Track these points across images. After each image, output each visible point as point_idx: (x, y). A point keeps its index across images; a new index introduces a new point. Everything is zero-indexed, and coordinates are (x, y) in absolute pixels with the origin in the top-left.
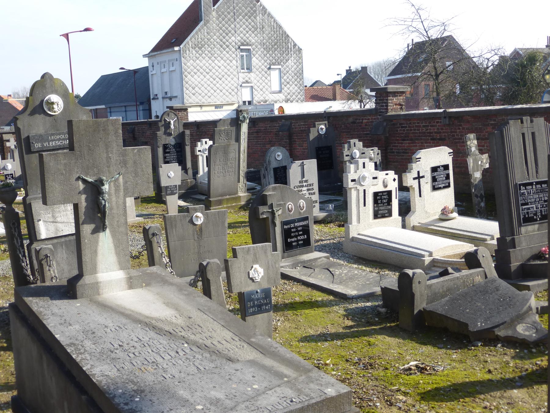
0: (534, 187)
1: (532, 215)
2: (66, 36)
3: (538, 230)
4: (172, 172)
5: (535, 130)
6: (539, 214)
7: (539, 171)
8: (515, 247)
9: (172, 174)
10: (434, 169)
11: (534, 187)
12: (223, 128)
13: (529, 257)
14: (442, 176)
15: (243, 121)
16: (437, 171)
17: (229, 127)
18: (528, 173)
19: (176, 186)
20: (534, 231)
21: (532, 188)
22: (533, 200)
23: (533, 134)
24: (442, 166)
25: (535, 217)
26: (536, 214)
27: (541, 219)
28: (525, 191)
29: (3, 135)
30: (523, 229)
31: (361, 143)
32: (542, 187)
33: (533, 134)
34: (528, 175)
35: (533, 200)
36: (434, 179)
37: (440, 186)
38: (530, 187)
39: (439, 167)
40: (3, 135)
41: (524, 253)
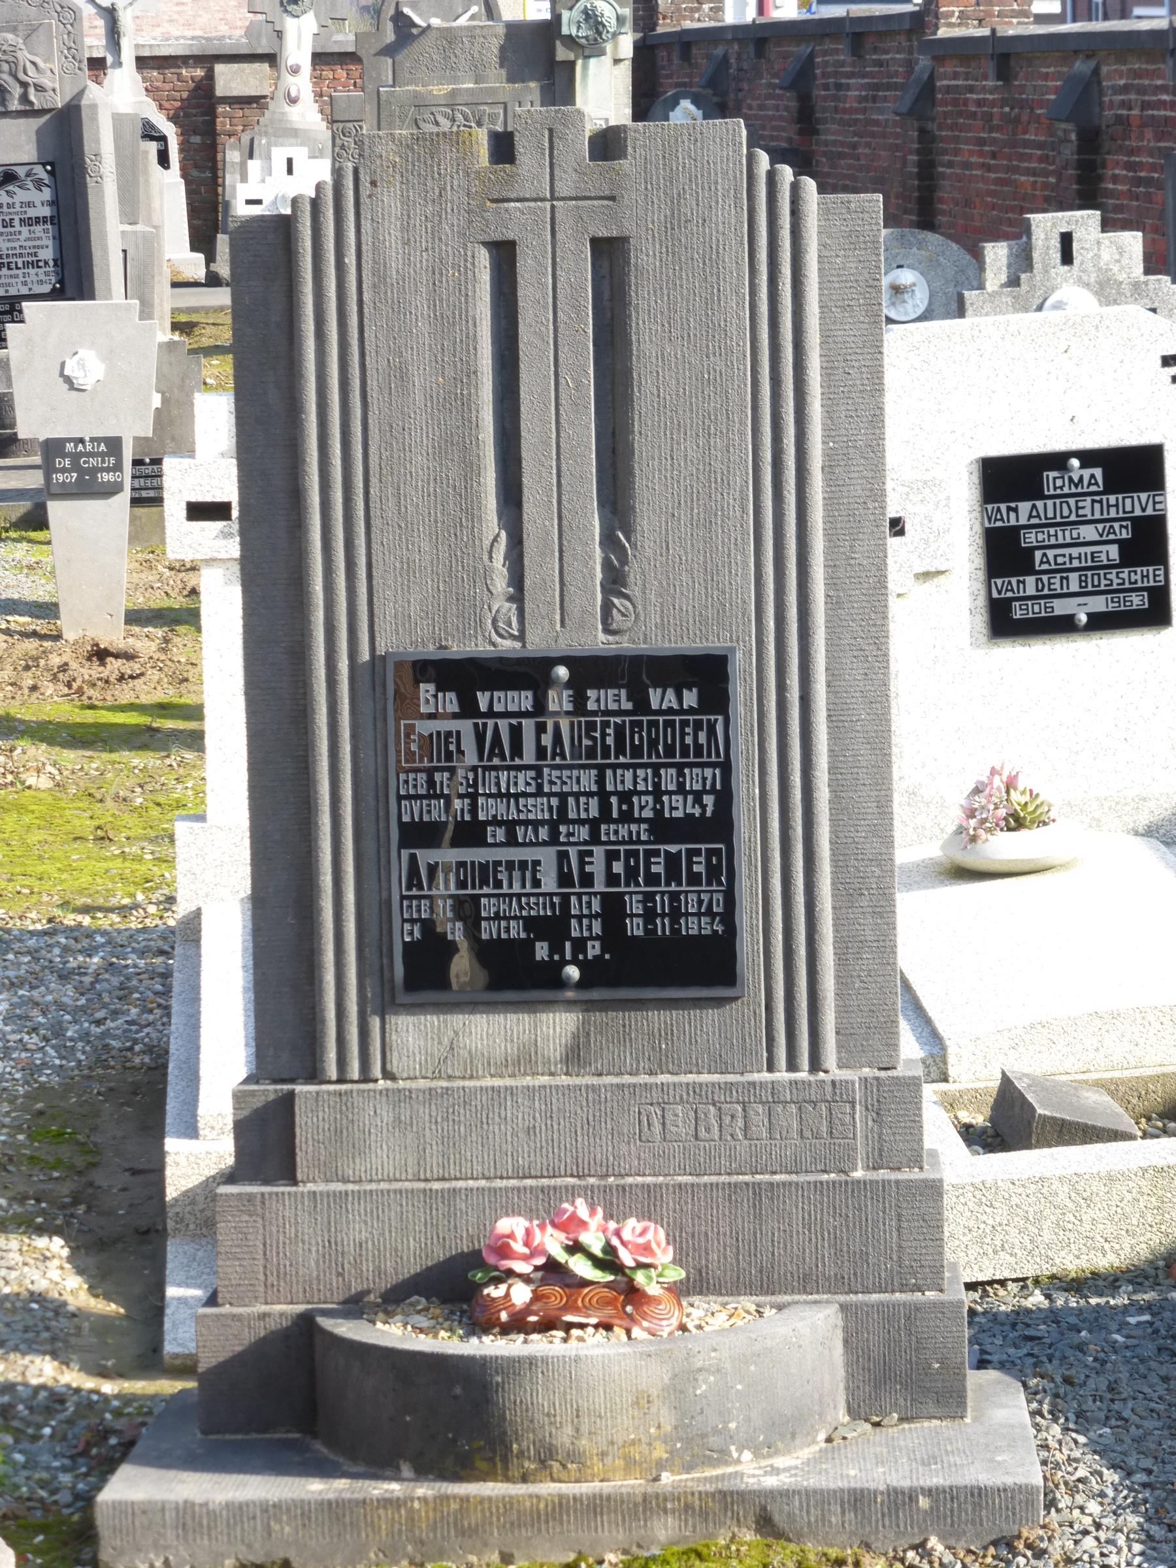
0: (559, 700)
1: (516, 931)
3: (576, 1056)
4: (88, 355)
5: (640, 221)
6: (587, 927)
7: (633, 572)
8: (290, 1175)
9: (89, 367)
10: (1008, 479)
11: (559, 700)
12: (440, 90)
13: (412, 1267)
14: (1088, 533)
15: (592, 47)
16: (1035, 492)
17: (496, 80)
18: (517, 579)
19: (114, 445)
20: (525, 1061)
21: (540, 707)
22: (538, 809)
23: (609, 254)
24: (1089, 458)
25: (542, 951)
26: (552, 928)
27: (593, 975)
28: (466, 727)
29: (219, 68)
30: (414, 1035)
31: (1133, 242)
32: (642, 705)
33: (609, 254)
34: (518, 596)
35: (538, 809)
36: (1004, 553)
37: (1061, 607)
38: (524, 700)
39: (1058, 461)
40: (219, 68)
41: (357, 1230)
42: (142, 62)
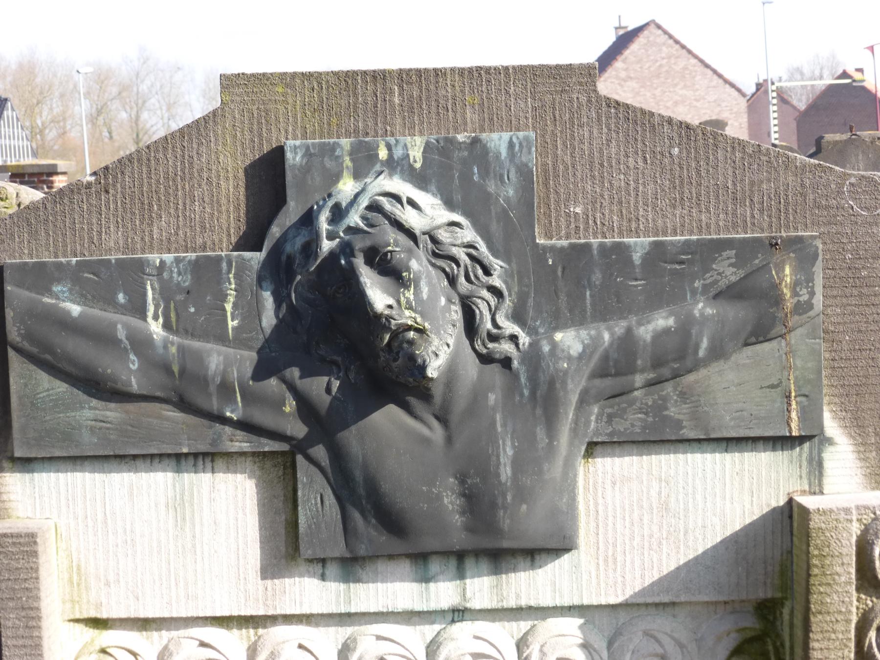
2: (871, 49)
42: (799, 301)
